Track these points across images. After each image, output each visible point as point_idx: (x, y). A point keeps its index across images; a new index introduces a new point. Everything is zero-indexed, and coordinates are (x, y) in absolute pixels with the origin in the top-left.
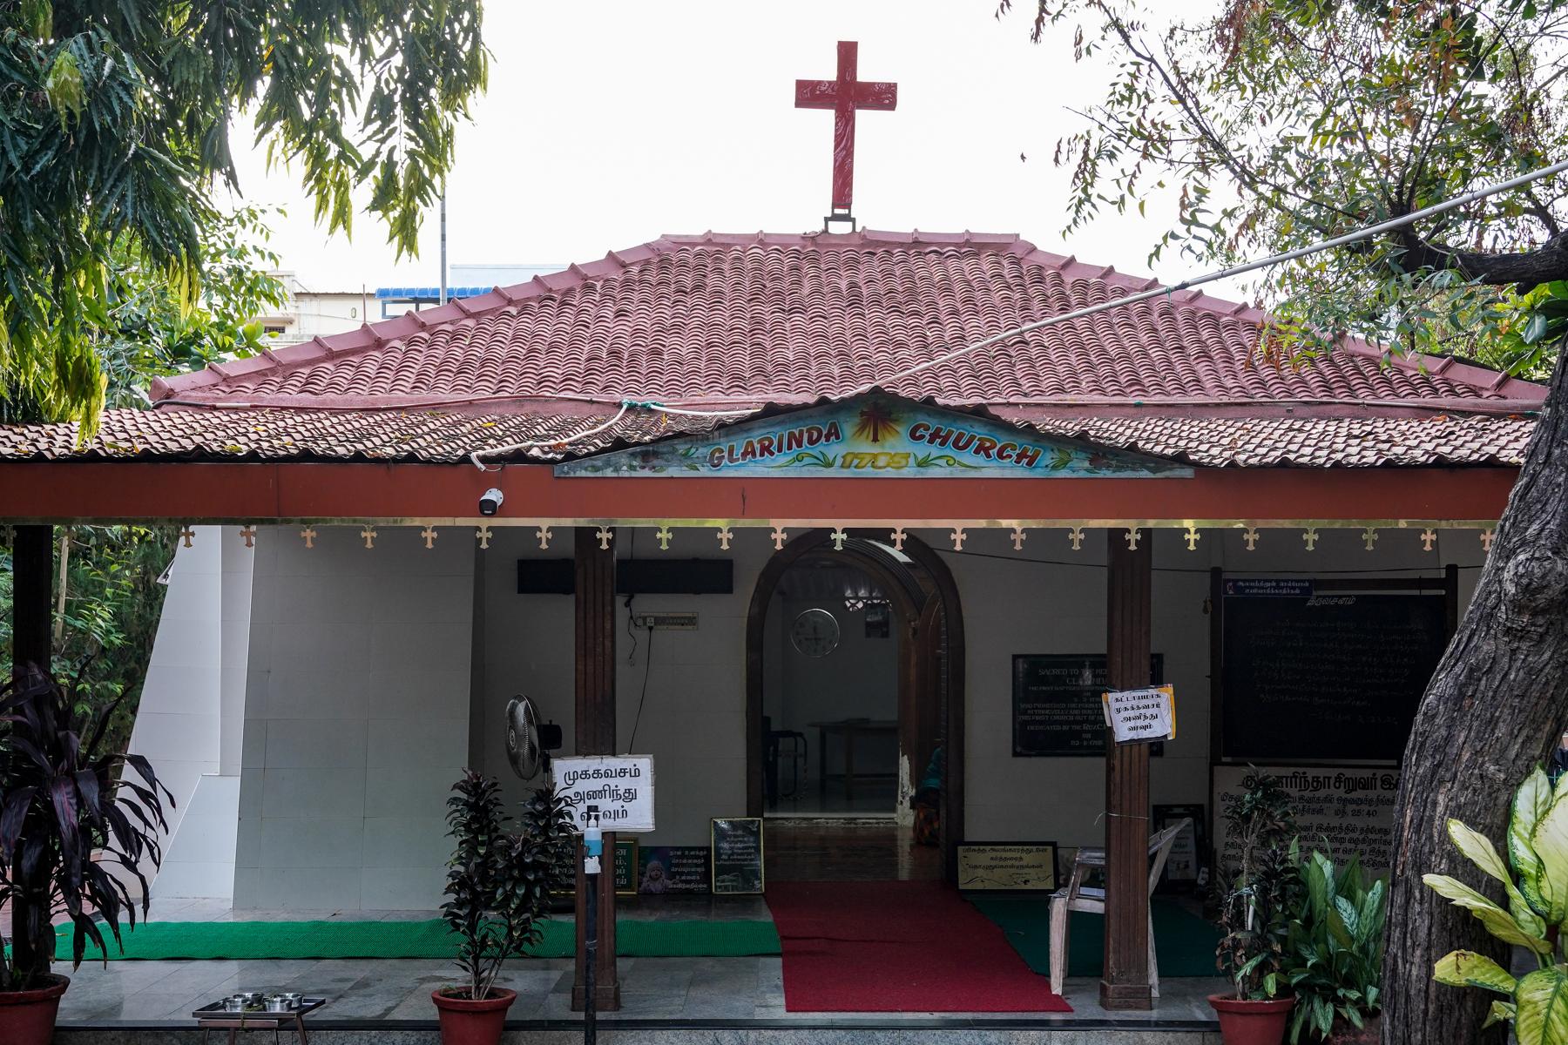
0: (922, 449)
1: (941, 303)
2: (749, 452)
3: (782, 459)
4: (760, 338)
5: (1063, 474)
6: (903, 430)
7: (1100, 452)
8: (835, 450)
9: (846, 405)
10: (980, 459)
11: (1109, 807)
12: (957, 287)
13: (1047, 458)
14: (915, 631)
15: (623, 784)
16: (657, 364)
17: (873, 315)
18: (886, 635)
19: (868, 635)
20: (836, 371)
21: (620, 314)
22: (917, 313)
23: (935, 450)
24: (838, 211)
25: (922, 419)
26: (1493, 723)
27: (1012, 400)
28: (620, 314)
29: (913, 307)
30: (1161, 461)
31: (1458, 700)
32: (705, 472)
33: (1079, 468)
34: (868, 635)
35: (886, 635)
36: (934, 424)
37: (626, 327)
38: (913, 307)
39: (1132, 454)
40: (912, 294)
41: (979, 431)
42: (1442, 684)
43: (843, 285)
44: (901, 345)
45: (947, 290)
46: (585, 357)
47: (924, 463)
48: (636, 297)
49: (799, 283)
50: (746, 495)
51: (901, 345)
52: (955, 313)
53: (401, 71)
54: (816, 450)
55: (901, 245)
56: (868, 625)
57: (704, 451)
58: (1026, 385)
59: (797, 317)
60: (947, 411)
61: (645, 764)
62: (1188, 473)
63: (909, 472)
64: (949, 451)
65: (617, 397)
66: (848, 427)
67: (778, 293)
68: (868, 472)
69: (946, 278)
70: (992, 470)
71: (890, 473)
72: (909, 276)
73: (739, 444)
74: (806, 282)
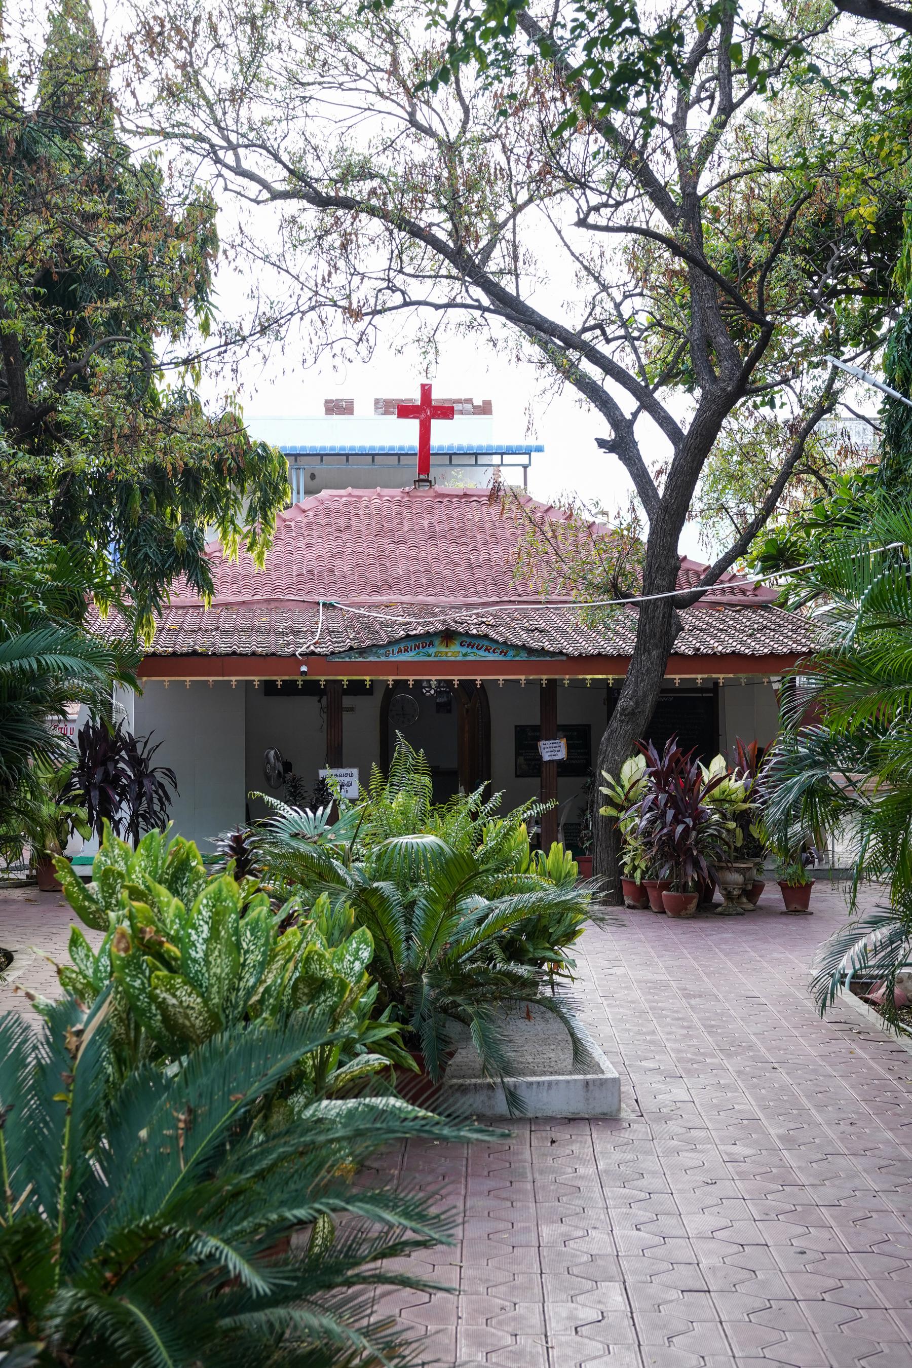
0: (465, 650)
1: (479, 536)
2: (400, 651)
3: (412, 654)
4: (383, 561)
5: (517, 659)
6: (457, 643)
7: (531, 651)
8: (432, 650)
9: (436, 634)
10: (486, 653)
11: (542, 788)
12: (488, 525)
13: (511, 653)
14: (467, 711)
15: (346, 780)
16: (332, 578)
17: (442, 544)
18: (449, 711)
19: (438, 712)
20: (424, 581)
21: (309, 546)
22: (465, 544)
23: (469, 650)
24: (422, 477)
25: (465, 639)
26: (616, 745)
27: (512, 599)
28: (309, 546)
29: (464, 540)
30: (553, 654)
31: (608, 739)
32: (383, 659)
33: (523, 656)
34: (438, 712)
35: (449, 711)
36: (469, 640)
37: (310, 555)
38: (464, 540)
39: (543, 651)
40: (463, 530)
41: (486, 643)
42: (606, 734)
43: (426, 523)
44: (457, 565)
45: (482, 529)
46: (294, 574)
47: (465, 655)
48: (315, 534)
49: (401, 523)
50: (398, 667)
51: (457, 565)
52: (486, 544)
53: (259, 498)
54: (425, 650)
55: (457, 496)
56: (438, 704)
57: (382, 651)
58: (520, 589)
59: (402, 547)
60: (473, 636)
61: (355, 771)
62: (564, 658)
63: (460, 658)
64: (475, 650)
65: (317, 598)
66: (437, 642)
67: (391, 531)
68: (444, 658)
69: (481, 520)
70: (491, 657)
71: (453, 659)
72: (461, 519)
73: (396, 649)
74: (405, 522)
